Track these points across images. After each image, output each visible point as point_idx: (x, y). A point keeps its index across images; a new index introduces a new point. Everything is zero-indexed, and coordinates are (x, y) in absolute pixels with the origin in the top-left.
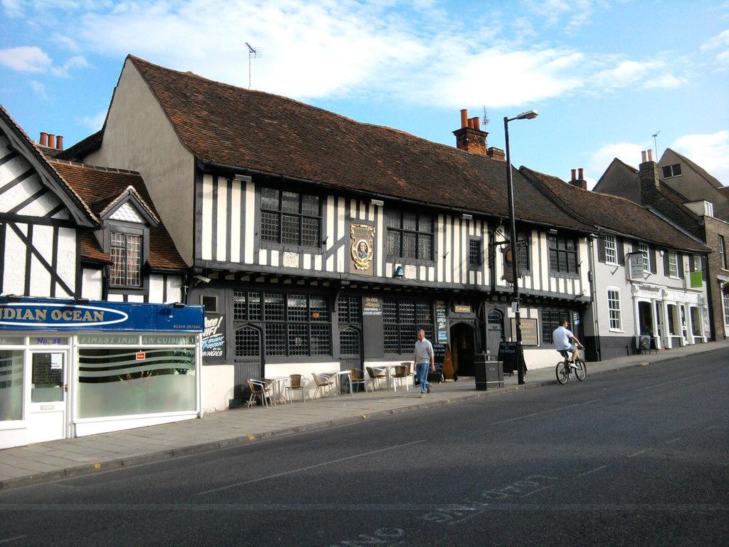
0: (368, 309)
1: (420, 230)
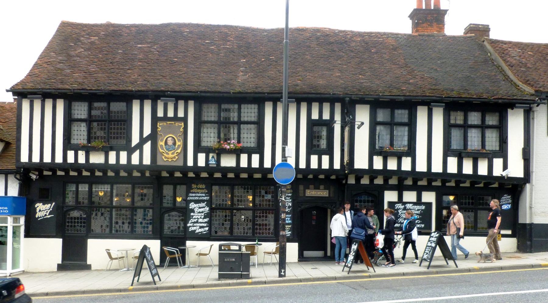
0: (194, 195)
1: (236, 119)
